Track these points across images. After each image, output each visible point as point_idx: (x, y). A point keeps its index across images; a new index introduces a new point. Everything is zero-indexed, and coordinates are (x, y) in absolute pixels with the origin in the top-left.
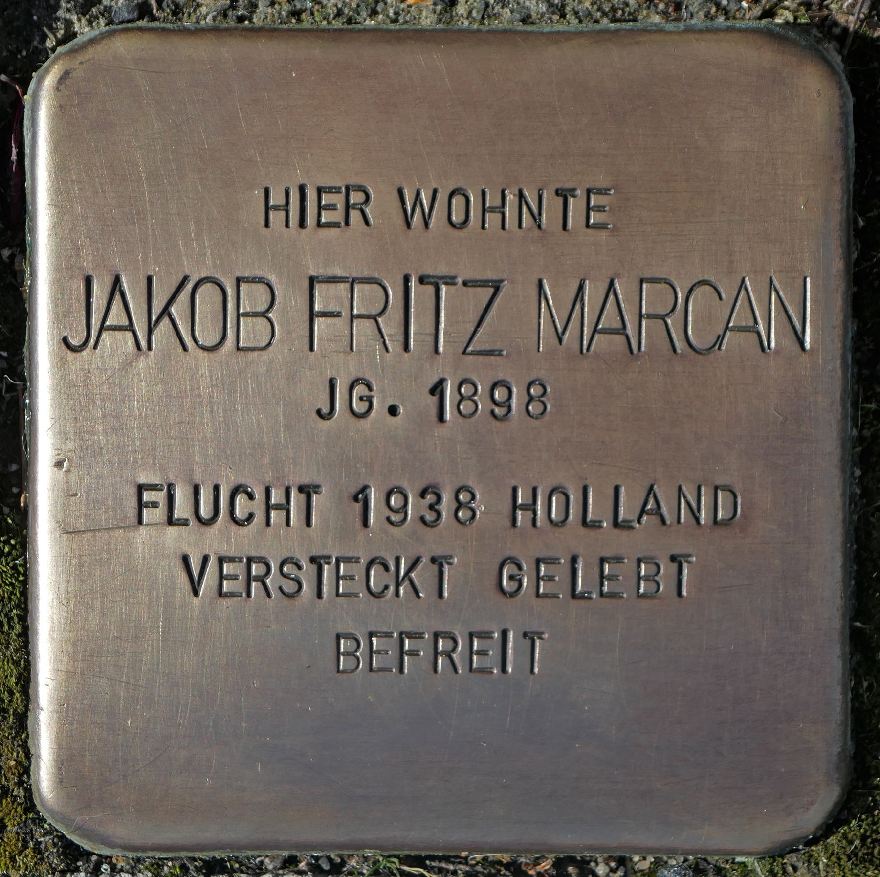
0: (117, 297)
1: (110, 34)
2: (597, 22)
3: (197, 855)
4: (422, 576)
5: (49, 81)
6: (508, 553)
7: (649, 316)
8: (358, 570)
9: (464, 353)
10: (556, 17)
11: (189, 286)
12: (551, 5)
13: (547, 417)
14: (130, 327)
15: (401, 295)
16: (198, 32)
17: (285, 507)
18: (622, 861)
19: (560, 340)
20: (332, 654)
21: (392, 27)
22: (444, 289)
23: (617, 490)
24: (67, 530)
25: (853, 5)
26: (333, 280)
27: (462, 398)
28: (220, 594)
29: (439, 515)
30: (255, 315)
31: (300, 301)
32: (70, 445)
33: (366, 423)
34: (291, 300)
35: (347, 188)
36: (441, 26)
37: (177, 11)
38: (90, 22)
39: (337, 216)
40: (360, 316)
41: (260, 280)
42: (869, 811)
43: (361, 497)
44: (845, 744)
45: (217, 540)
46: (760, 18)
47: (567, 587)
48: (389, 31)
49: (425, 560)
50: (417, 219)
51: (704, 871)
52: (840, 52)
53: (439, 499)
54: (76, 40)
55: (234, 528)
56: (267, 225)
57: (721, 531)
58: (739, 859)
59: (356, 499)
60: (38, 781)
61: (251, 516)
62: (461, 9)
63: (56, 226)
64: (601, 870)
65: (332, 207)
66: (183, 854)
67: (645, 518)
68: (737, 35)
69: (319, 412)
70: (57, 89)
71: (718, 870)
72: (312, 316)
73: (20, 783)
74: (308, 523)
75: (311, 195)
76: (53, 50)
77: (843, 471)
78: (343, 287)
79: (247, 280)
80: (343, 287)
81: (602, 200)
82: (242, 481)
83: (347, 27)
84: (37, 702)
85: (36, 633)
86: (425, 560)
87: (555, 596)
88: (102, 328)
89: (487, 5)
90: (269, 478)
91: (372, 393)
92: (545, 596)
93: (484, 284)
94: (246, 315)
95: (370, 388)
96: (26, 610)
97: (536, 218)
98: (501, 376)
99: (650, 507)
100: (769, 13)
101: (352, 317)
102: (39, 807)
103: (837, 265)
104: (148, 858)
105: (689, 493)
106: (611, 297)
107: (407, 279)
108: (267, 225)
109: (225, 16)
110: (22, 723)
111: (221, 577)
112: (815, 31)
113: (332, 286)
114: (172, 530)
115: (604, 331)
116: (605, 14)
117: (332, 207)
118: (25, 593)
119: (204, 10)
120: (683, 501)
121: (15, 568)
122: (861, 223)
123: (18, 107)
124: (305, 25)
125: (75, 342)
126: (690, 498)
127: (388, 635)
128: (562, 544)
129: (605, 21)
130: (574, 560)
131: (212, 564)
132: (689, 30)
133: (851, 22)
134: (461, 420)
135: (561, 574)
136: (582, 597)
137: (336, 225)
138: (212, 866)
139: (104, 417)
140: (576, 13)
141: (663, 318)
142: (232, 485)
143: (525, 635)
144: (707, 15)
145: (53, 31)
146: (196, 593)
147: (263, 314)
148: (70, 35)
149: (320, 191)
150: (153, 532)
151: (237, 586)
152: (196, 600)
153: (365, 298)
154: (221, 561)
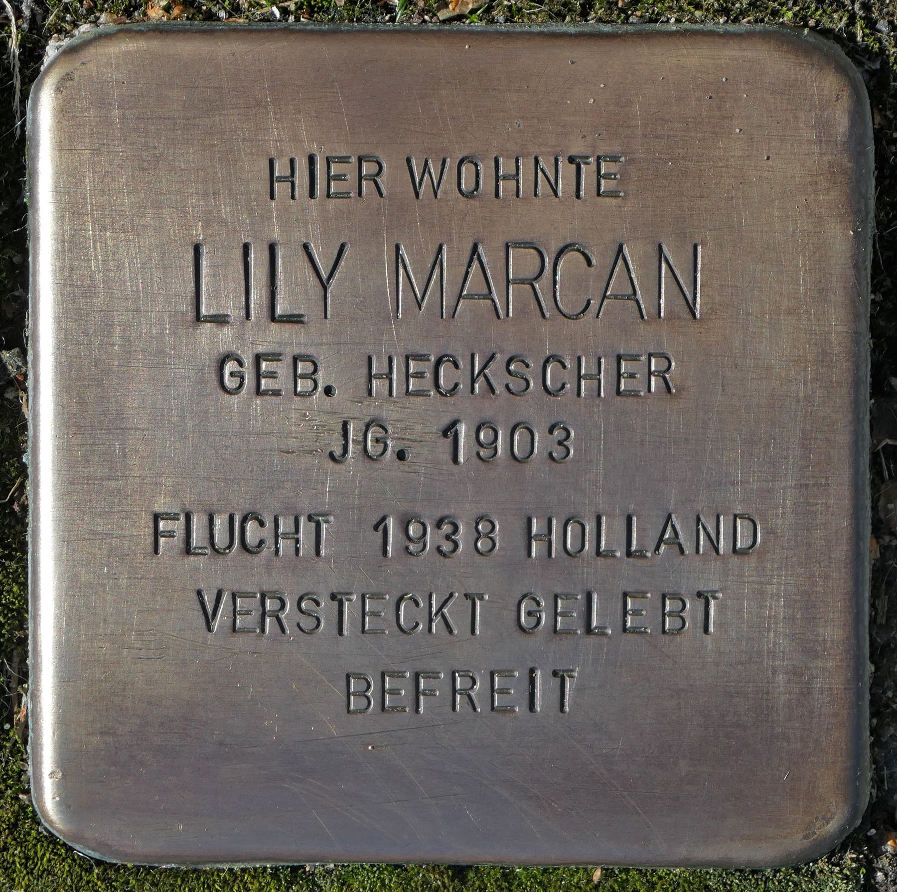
29: (456, 545)
53: (456, 529)
81: (613, 168)
91: (243, 369)
120: (702, 532)
126: (709, 529)
131: (226, 597)
149: (328, 161)
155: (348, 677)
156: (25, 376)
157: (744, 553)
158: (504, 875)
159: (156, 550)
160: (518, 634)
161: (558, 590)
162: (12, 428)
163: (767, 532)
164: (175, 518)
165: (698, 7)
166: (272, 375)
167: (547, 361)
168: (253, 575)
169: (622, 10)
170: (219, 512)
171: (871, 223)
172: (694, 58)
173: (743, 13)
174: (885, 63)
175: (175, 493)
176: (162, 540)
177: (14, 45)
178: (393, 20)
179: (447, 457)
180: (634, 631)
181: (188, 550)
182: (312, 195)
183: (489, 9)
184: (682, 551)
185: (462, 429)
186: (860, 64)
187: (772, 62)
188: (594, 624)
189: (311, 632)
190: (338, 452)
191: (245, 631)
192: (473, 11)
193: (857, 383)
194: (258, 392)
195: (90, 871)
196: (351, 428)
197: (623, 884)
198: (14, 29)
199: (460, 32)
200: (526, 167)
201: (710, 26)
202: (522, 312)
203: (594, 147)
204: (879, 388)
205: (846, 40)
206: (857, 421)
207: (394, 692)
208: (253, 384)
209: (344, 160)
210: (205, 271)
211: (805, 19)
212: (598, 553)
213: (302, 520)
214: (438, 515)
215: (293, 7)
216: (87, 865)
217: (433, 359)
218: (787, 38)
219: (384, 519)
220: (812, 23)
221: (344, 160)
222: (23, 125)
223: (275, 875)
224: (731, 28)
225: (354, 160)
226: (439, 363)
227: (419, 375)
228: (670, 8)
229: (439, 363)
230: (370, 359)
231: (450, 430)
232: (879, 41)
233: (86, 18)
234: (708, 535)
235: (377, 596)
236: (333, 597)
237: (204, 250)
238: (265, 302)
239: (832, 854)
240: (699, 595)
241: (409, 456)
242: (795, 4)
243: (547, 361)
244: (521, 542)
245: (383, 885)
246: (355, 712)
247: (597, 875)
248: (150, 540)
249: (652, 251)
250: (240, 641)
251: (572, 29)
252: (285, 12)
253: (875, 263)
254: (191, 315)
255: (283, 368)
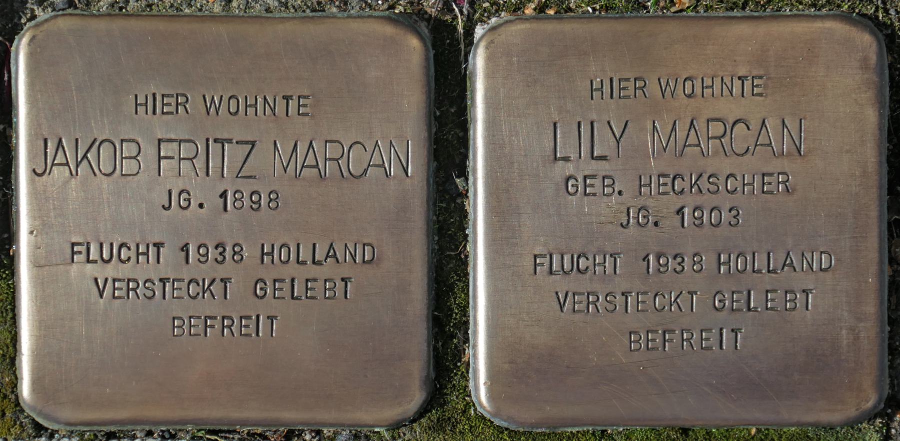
0: (60, 149)
1: (56, 17)
2: (304, 11)
3: (103, 428)
4: (217, 288)
5: (25, 41)
6: (259, 277)
7: (330, 159)
9: (253, 144)
10: (283, 9)
11: (97, 143)
12: (281, 2)
13: (279, 209)
14: (67, 164)
15: (205, 148)
16: (100, 16)
17: (146, 254)
18: (318, 432)
19: (285, 171)
20: (171, 327)
21: (199, 14)
22: (226, 145)
23: (314, 245)
24: (36, 264)
25: (434, 4)
26: (170, 141)
27: (236, 200)
28: (114, 297)
29: (225, 258)
30: (131, 158)
31: (153, 151)
32: (37, 223)
33: (186, 212)
34: (149, 150)
35: (177, 95)
36: (224, 13)
37: (88, 4)
38: (44, 10)
39: (172, 109)
40: (184, 159)
41: (133, 141)
42: (442, 406)
43: (185, 248)
44: (429, 371)
45: (110, 271)
46: (388, 9)
47: (290, 294)
48: (197, 16)
49: (218, 280)
50: (213, 110)
51: (360, 437)
52: (427, 27)
53: (225, 250)
54: (37, 20)
55: (121, 265)
56: (136, 113)
57: (367, 266)
58: (376, 430)
59: (182, 250)
60: (21, 391)
61: (129, 259)
62: (234, 4)
63: (29, 113)
64: (308, 437)
65: (169, 104)
66: (95, 428)
67: (328, 260)
68: (373, 20)
69: (163, 206)
70: (29, 45)
71: (367, 437)
72: (160, 158)
73: (13, 392)
74: (158, 262)
75: (159, 98)
76: (25, 24)
77: (428, 236)
78: (175, 145)
79: (126, 141)
80: (175, 145)
82: (125, 241)
83: (176, 13)
84: (20, 351)
85: (20, 317)
86: (218, 280)
87: (284, 298)
88: (53, 165)
89: (248, 2)
90: (138, 240)
92: (278, 298)
93: (247, 143)
94: (126, 158)
95: (189, 195)
96: (14, 306)
97: (273, 110)
98: (255, 189)
99: (331, 253)
100: (392, 7)
101: (180, 159)
102: (22, 404)
103: (424, 134)
106: (311, 150)
107: (208, 140)
108: (136, 113)
109: (113, 7)
110: (12, 361)
111: (114, 289)
112: (414, 17)
113: (170, 144)
114: (89, 266)
115: (307, 166)
116: (308, 7)
117: (169, 104)
118: (14, 298)
119: (102, 3)
121: (8, 285)
122: (438, 114)
123: (8, 53)
124: (154, 12)
125: (39, 171)
127: (199, 317)
128: (287, 272)
129: (308, 11)
130: (293, 280)
131: (570, 295)
132: (349, 17)
133: (433, 12)
134: (236, 210)
135: (287, 286)
136: (297, 298)
137: (172, 113)
138: (110, 435)
139: (54, 209)
140: (294, 7)
141: (337, 160)
142: (120, 243)
143: (268, 317)
144: (361, 8)
145: (25, 14)
146: (101, 297)
147: (135, 158)
148: (34, 17)
149: (163, 96)
150: (79, 265)
151: (123, 293)
152: (101, 301)
153: (186, 150)
154: (114, 280)
155: (630, 333)
156: (467, 191)
157: (826, 270)
158: (707, 433)
159: (535, 273)
160: (714, 311)
161: (734, 289)
162: (460, 217)
163: (837, 260)
164: (544, 256)
165: (801, 3)
166: (592, 186)
167: (728, 177)
168: (584, 284)
169: (763, 6)
170: (566, 253)
171: (887, 110)
172: (800, 28)
173: (823, 6)
174: (893, 30)
175: (545, 245)
176: (538, 268)
177: (460, 29)
178: (649, 12)
179: (679, 224)
180: (772, 309)
181: (551, 272)
182: (612, 97)
183: (695, 7)
184: (795, 270)
185: (686, 210)
186: (882, 31)
187: (839, 28)
188: (752, 306)
189: (612, 311)
190: (625, 223)
191: (579, 311)
192: (688, 7)
193: (880, 188)
194: (585, 194)
195: (502, 433)
196: (631, 211)
197: (766, 436)
198: (460, 20)
199: (684, 17)
200: (718, 81)
201: (807, 12)
202: (716, 153)
203: (750, 71)
204: (891, 191)
205: (874, 19)
206: (881, 206)
207: (653, 340)
208: (583, 190)
209: (627, 80)
210: (558, 136)
211: (853, 9)
212: (754, 271)
213: (607, 257)
214: (674, 253)
215: (598, 7)
216: (500, 430)
217: (671, 176)
218: (846, 18)
219: (648, 255)
220: (857, 11)
221: (627, 80)
222: (466, 68)
223: (593, 434)
224: (817, 13)
225: (632, 80)
226: (674, 178)
227: (665, 184)
228: (787, 4)
229: (674, 178)
230: (640, 177)
231: (680, 211)
232: (891, 19)
233: (494, 15)
234: (808, 262)
235: (645, 293)
236: (623, 294)
237: (558, 125)
238: (589, 150)
239: (870, 420)
240: (804, 291)
241: (660, 224)
242: (849, 1)
243: (728, 177)
244: (715, 265)
245: (647, 438)
246: (634, 350)
247: (753, 431)
248: (533, 267)
249: (779, 122)
250: (577, 317)
251: (739, 15)
252: (594, 9)
253: (889, 128)
254: (552, 157)
255: (598, 182)
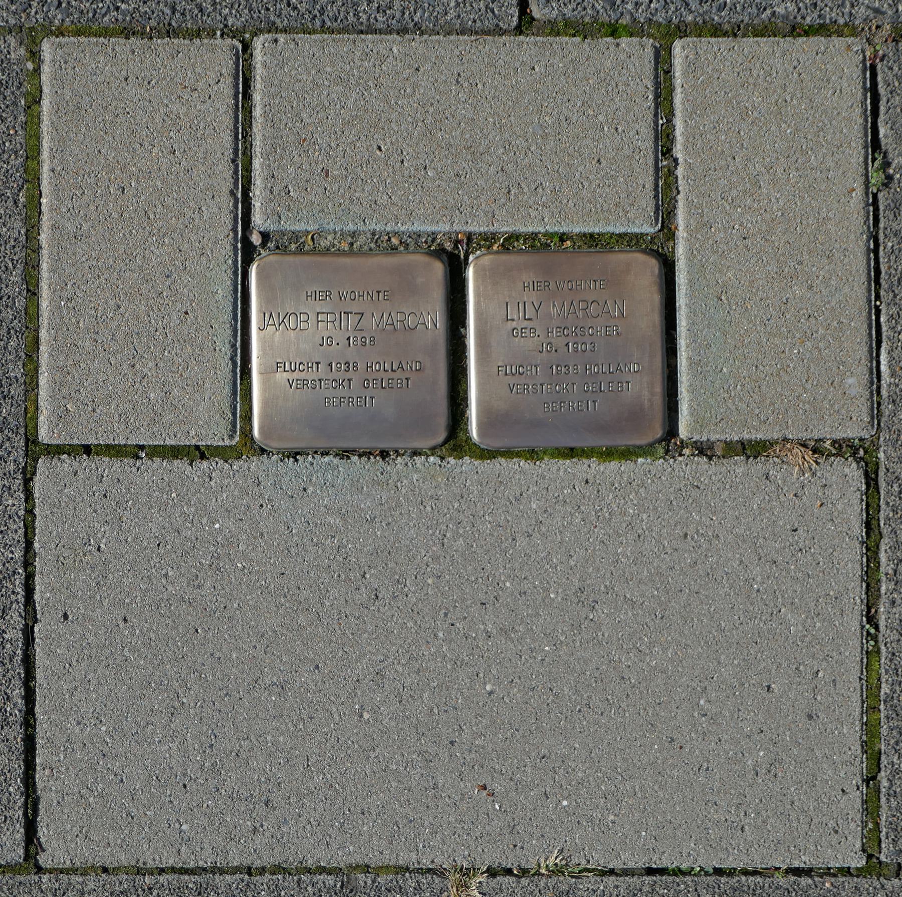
8: (330, 382)
24: (261, 373)
34: (313, 317)
43: (330, 365)
45: (296, 375)
97: (372, 298)
99: (401, 367)
104: (556, 858)
105: (410, 363)
128: (382, 374)
148: (260, 254)
